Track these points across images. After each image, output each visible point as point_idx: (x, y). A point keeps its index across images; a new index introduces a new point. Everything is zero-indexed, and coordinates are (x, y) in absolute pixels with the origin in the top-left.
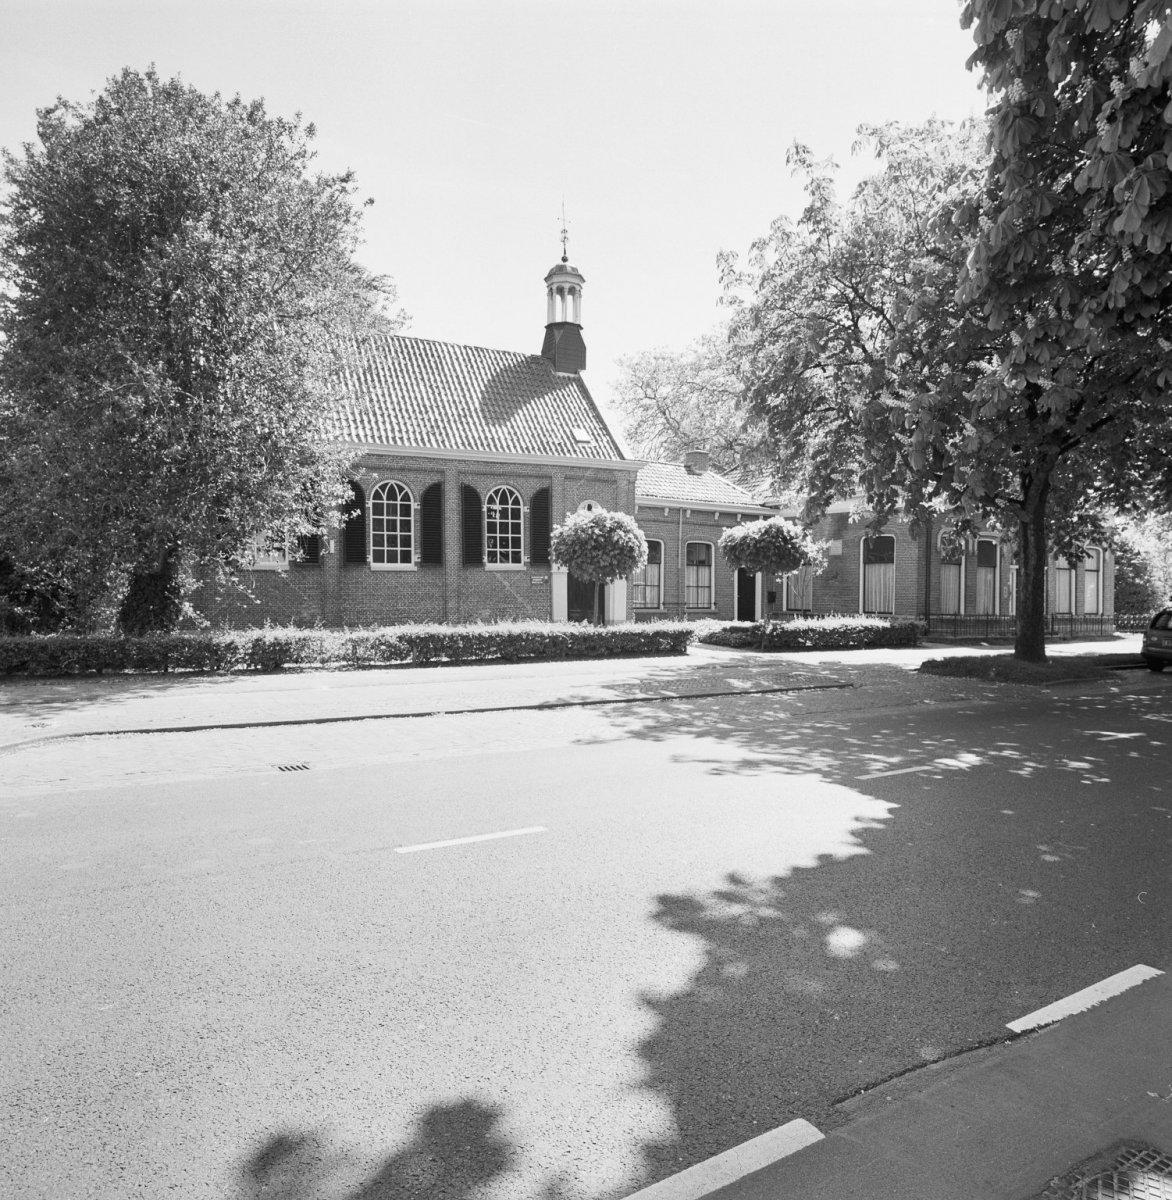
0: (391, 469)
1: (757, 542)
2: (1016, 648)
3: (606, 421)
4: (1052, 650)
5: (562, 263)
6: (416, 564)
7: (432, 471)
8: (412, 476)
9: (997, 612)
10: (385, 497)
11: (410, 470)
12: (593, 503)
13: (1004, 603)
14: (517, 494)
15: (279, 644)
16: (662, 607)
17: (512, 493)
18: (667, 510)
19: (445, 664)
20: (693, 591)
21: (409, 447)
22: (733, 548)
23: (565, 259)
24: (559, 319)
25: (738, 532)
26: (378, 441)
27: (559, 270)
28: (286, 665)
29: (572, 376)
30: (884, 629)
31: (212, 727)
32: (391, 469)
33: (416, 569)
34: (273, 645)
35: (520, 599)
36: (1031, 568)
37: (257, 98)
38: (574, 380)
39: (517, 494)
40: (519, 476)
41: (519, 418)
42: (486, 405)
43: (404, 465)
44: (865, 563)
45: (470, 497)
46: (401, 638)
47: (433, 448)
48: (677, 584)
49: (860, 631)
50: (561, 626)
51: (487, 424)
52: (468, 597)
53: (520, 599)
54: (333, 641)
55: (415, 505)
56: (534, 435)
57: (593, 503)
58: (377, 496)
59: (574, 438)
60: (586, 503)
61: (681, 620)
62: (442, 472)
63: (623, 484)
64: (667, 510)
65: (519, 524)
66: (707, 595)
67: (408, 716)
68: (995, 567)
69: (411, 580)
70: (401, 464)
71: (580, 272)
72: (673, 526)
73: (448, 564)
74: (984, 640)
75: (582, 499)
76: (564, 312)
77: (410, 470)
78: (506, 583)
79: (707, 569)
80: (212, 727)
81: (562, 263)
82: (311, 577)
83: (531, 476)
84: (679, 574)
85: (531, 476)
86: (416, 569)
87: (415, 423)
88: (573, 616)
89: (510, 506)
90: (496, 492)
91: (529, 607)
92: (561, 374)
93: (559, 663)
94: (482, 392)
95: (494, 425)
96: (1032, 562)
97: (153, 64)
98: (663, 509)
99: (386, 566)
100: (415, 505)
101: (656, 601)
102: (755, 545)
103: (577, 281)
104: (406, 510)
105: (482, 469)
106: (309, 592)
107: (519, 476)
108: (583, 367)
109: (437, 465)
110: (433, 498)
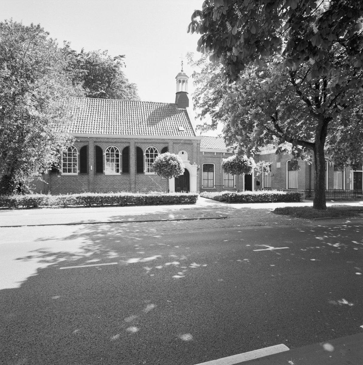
0: (112, 142)
1: (232, 163)
2: (314, 203)
3: (192, 124)
4: (328, 205)
5: (181, 72)
6: (121, 173)
7: (126, 142)
8: (119, 144)
9: (344, 189)
10: (149, 152)
11: (118, 142)
12: (185, 152)
13: (347, 185)
14: (156, 149)
15: (32, 200)
16: (214, 187)
17: (154, 149)
18: (215, 153)
19: (117, 206)
20: (227, 181)
21: (118, 135)
22: (225, 165)
23: (182, 71)
24: (180, 91)
25: (225, 160)
26: (145, 134)
27: (180, 74)
28: (40, 206)
29: (183, 109)
30: (283, 195)
31: (55, 225)
32: (112, 142)
33: (120, 175)
34: (30, 199)
35: (157, 184)
36: (318, 170)
37: (38, 24)
38: (184, 111)
39: (156, 149)
40: (157, 143)
41: (160, 125)
42: (149, 120)
43: (116, 141)
44: (288, 171)
45: (139, 151)
46: (77, 198)
47: (126, 136)
48: (221, 179)
49: (272, 196)
50: (173, 193)
51: (148, 127)
52: (139, 184)
53: (157, 184)
54: (52, 198)
55: (120, 154)
56: (169, 129)
57: (185, 152)
58: (147, 151)
59: (178, 130)
60: (181, 151)
61: (95, 193)
62: (129, 143)
63: (195, 144)
64: (215, 153)
65: (119, 159)
66: (232, 183)
67: (10, 227)
68: (213, 172)
69: (118, 178)
70: (115, 140)
71: (186, 75)
72: (218, 159)
73: (131, 173)
74: (333, 200)
75: (180, 150)
76: (182, 88)
77: (118, 142)
78: (152, 179)
79: (212, 173)
80: (55, 225)
81: (181, 72)
82: (85, 177)
83: (161, 143)
84: (221, 176)
85: (161, 143)
86: (120, 175)
87: (122, 127)
88: (176, 190)
89: (154, 153)
90: (149, 149)
91: (160, 187)
92: (180, 109)
93: (139, 207)
94: (149, 116)
95: (150, 127)
96: (319, 168)
97: (12, 18)
98: (214, 153)
99: (67, 174)
100: (120, 154)
101: (212, 185)
102: (231, 164)
103: (186, 78)
104: (117, 156)
105: (143, 141)
106: (84, 182)
107: (157, 143)
108: (188, 106)
109: (128, 141)
110: (126, 151)
